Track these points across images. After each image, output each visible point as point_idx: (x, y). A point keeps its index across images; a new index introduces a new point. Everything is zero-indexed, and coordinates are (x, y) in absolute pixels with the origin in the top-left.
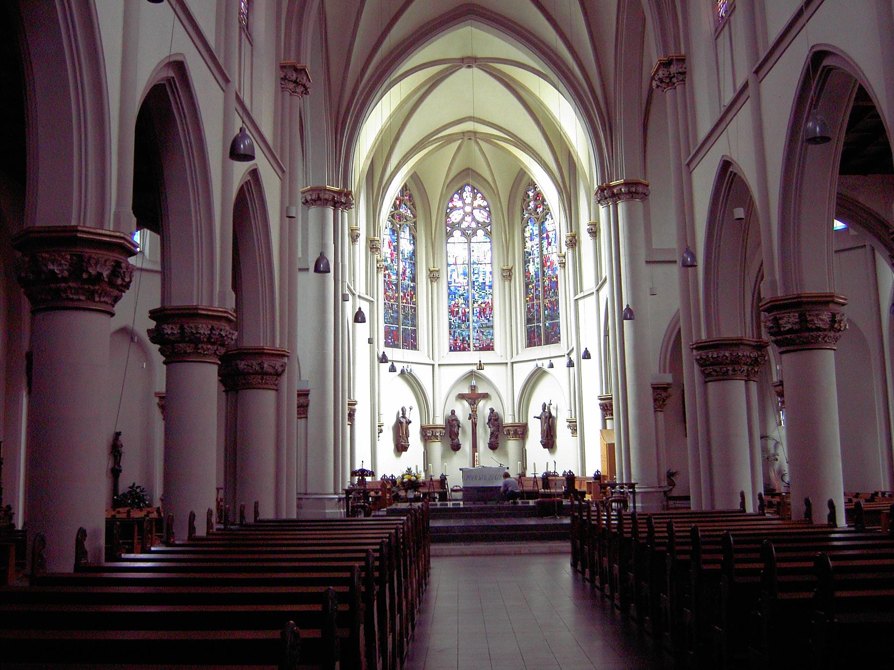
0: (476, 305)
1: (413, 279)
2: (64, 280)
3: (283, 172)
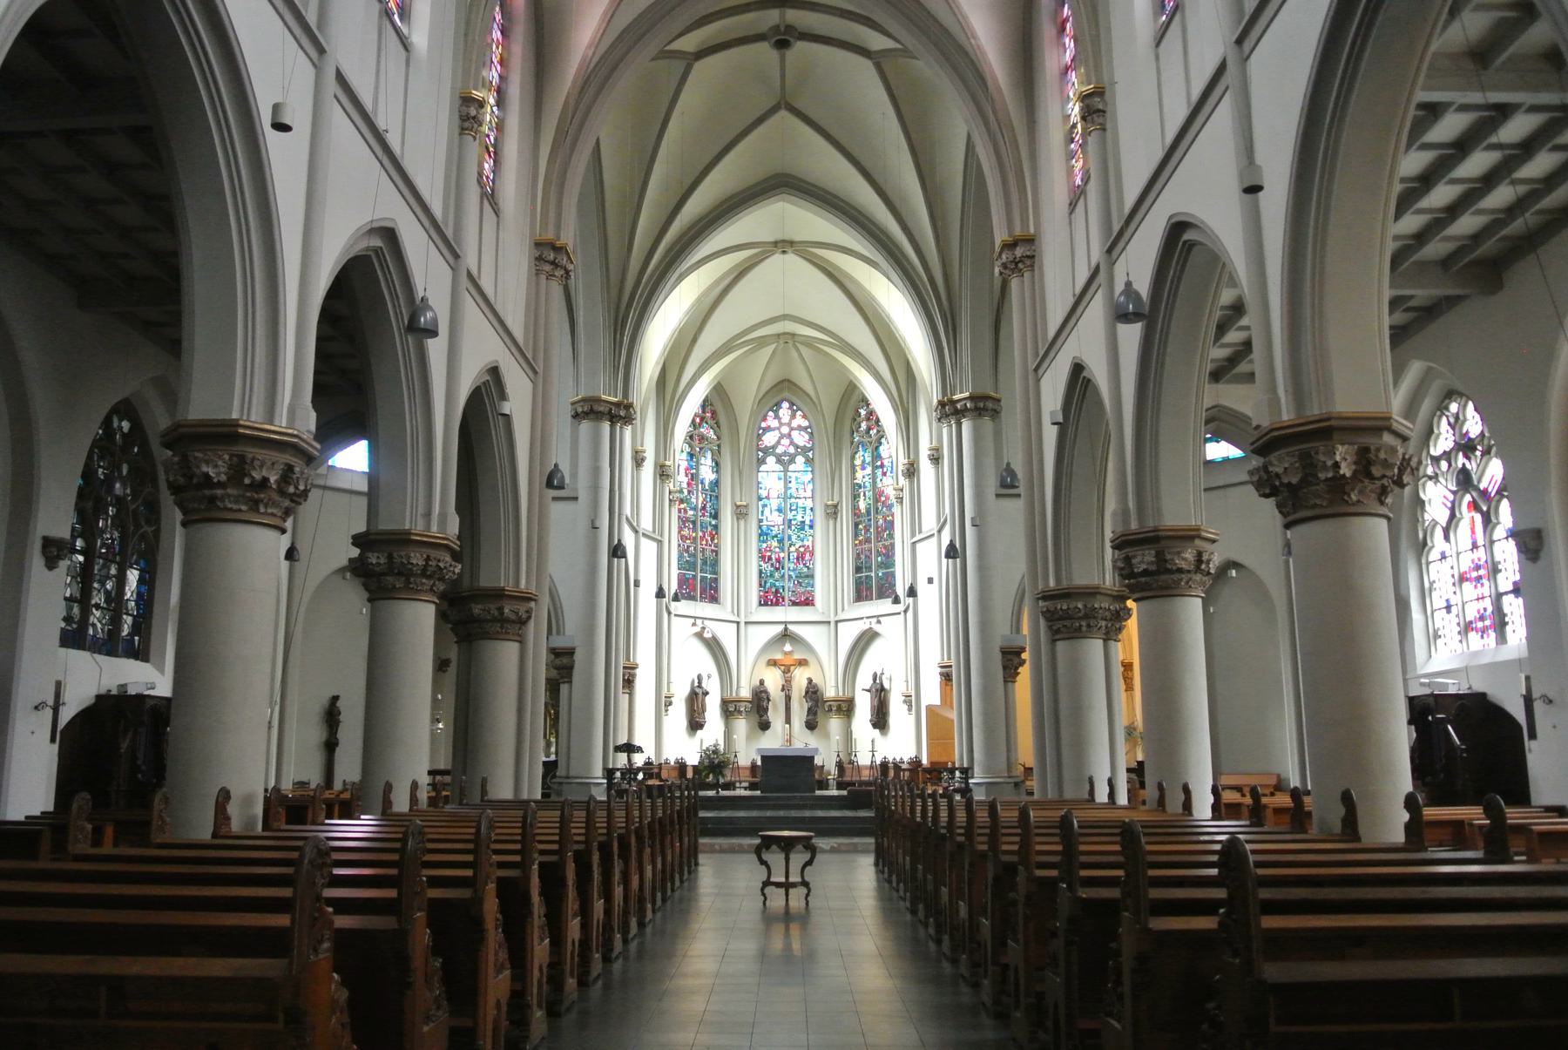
1: (715, 516)
2: (220, 485)
3: (535, 372)
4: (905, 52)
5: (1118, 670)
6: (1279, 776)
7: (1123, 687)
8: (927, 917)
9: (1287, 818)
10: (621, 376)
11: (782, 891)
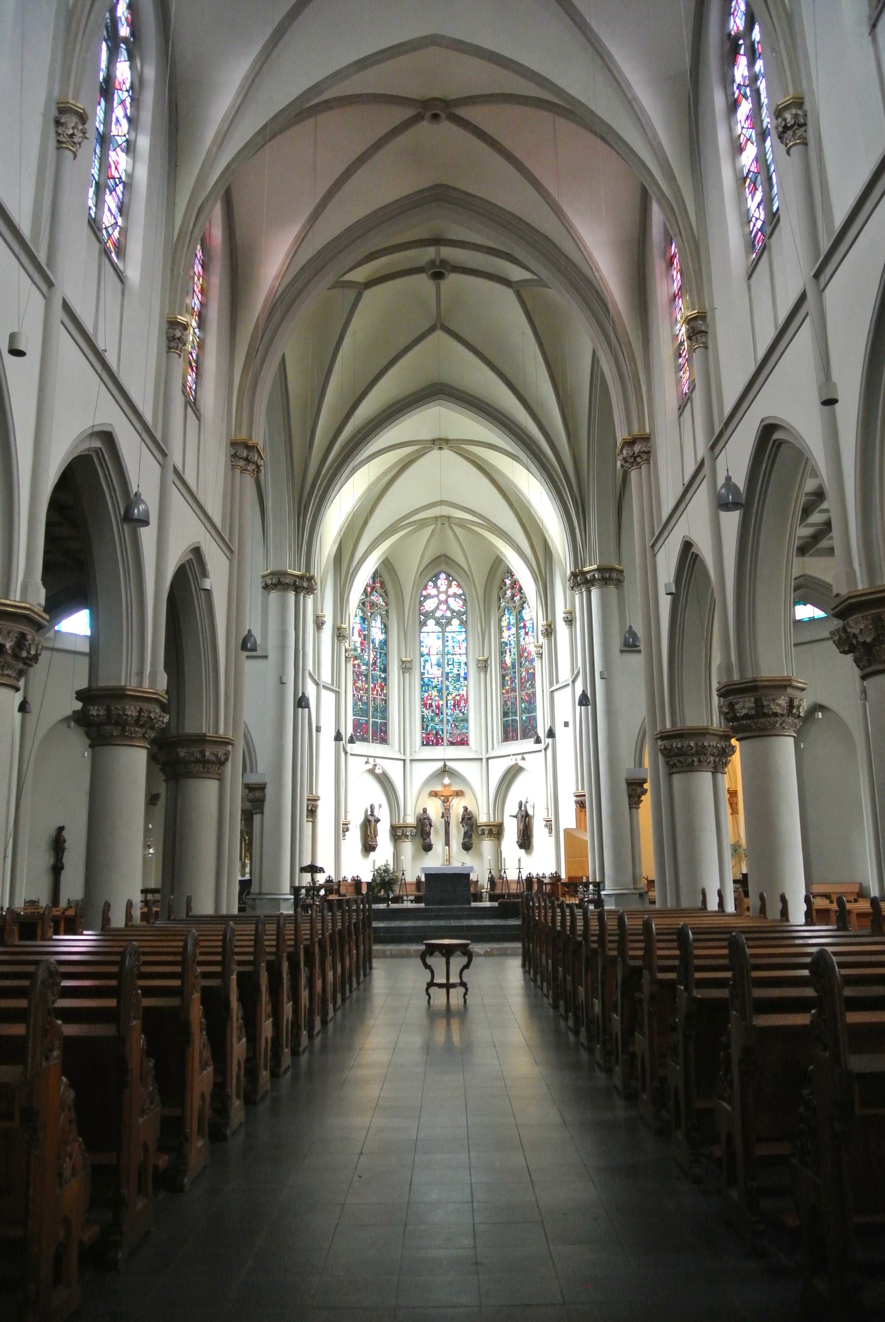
0: (450, 697)
1: (385, 670)
3: (232, 552)
4: (540, 283)
5: (725, 797)
6: (861, 884)
7: (729, 811)
8: (567, 1012)
9: (867, 922)
10: (304, 552)
11: (444, 990)
